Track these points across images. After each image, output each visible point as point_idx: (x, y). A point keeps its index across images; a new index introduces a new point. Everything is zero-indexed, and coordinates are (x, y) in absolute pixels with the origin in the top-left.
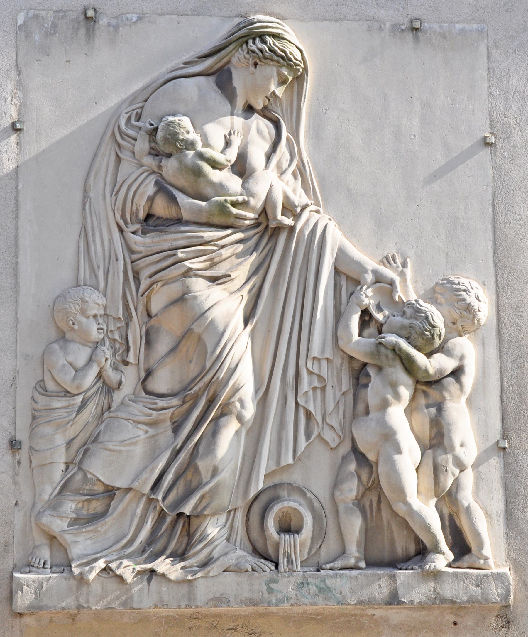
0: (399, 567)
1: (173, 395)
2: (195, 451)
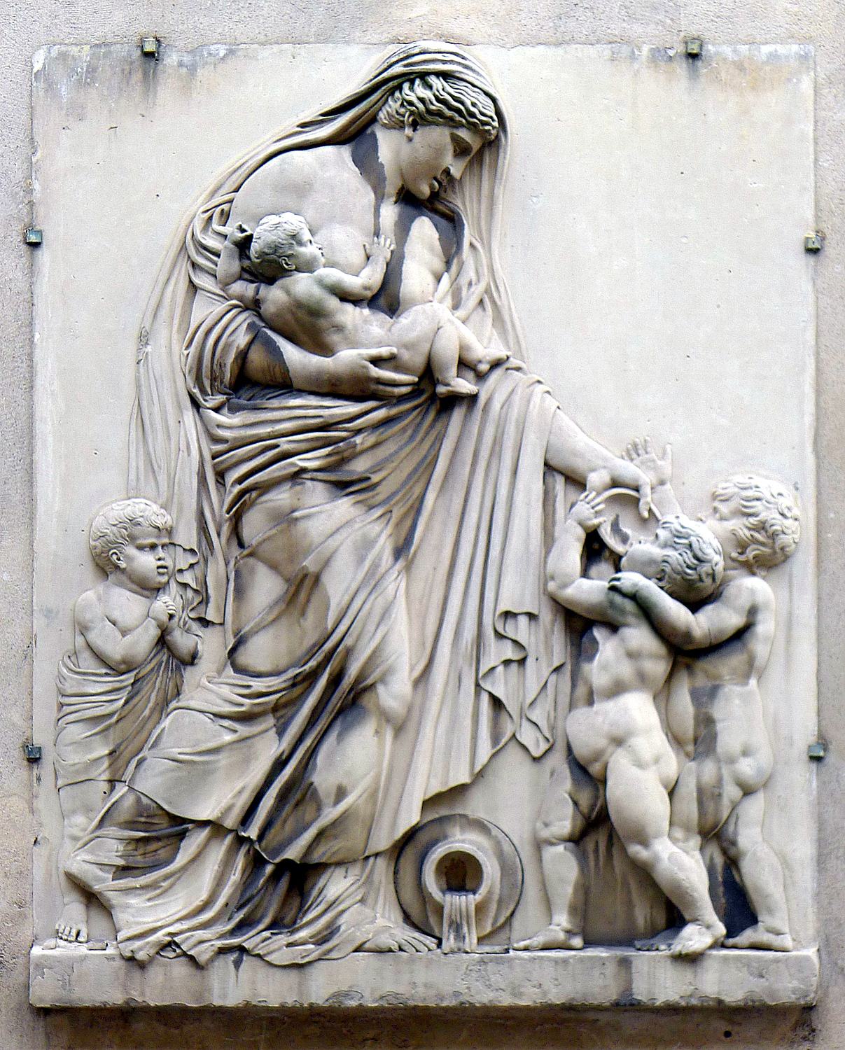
0: (639, 947)
2: (311, 763)
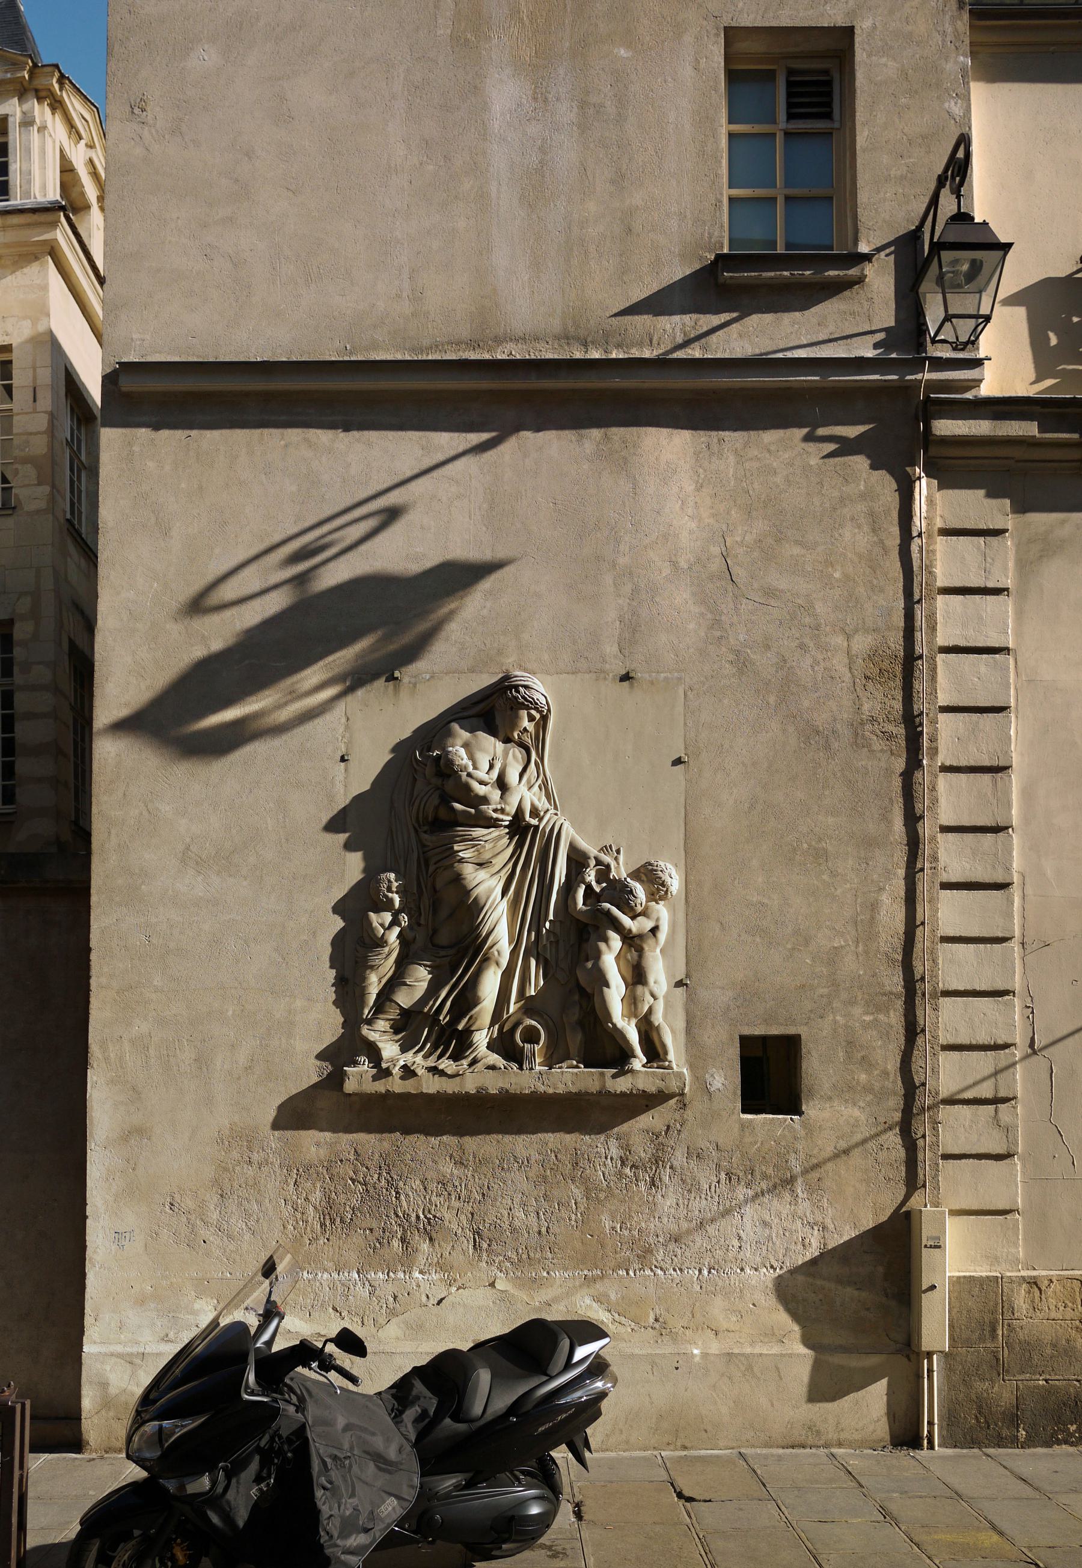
1: (451, 947)
